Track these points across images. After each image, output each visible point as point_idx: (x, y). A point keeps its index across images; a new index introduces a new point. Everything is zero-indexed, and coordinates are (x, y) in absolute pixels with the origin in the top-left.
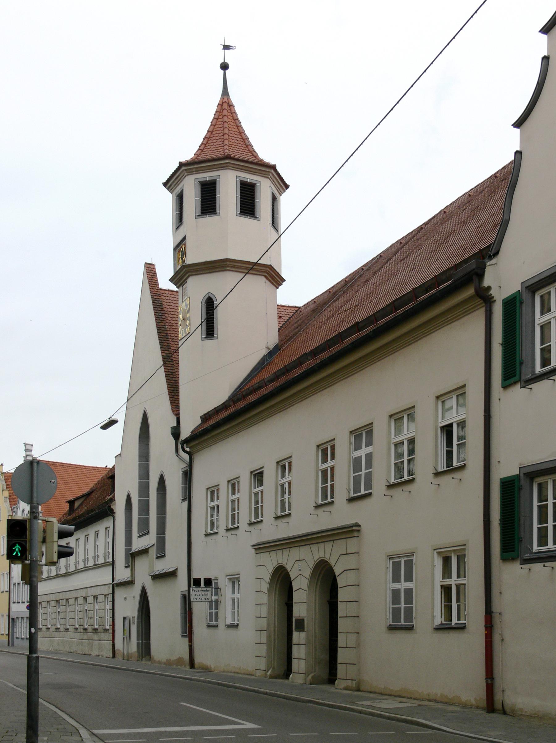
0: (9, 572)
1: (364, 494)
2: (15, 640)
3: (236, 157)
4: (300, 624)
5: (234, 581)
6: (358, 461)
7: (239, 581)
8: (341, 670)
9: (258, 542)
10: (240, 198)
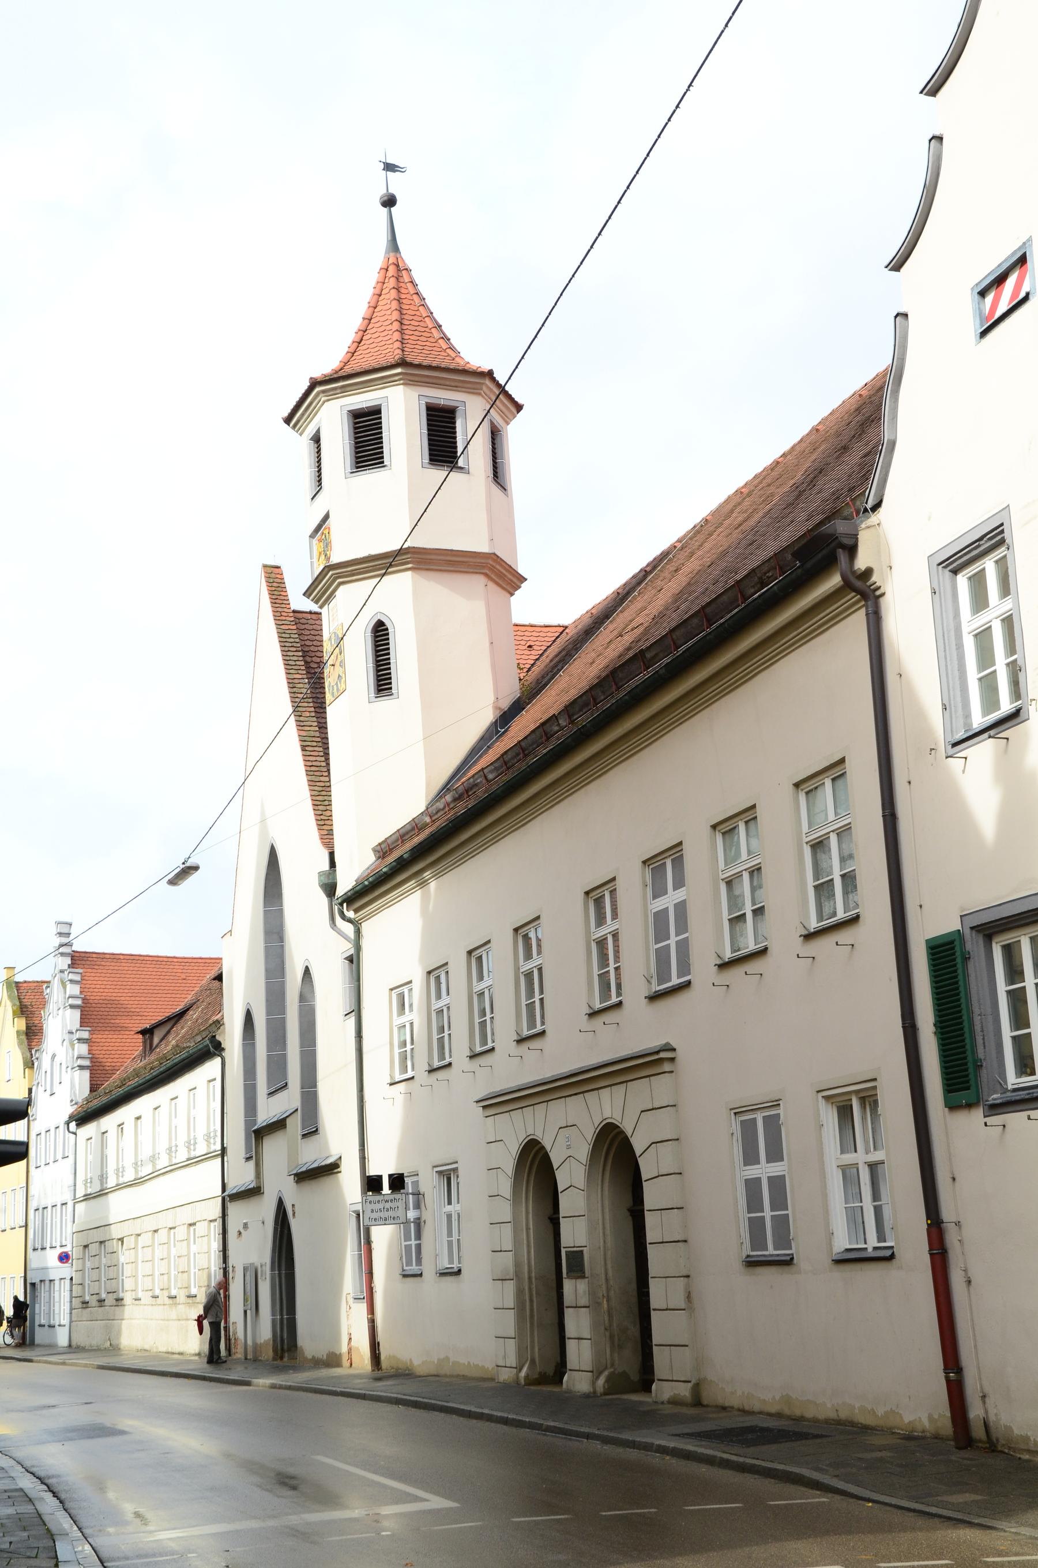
0: (25, 1185)
1: (678, 984)
2: (37, 1328)
3: (416, 362)
4: (576, 1258)
5: (448, 1176)
6: (661, 917)
7: (458, 1177)
8: (660, 1358)
9: (487, 1093)
10: (429, 435)
